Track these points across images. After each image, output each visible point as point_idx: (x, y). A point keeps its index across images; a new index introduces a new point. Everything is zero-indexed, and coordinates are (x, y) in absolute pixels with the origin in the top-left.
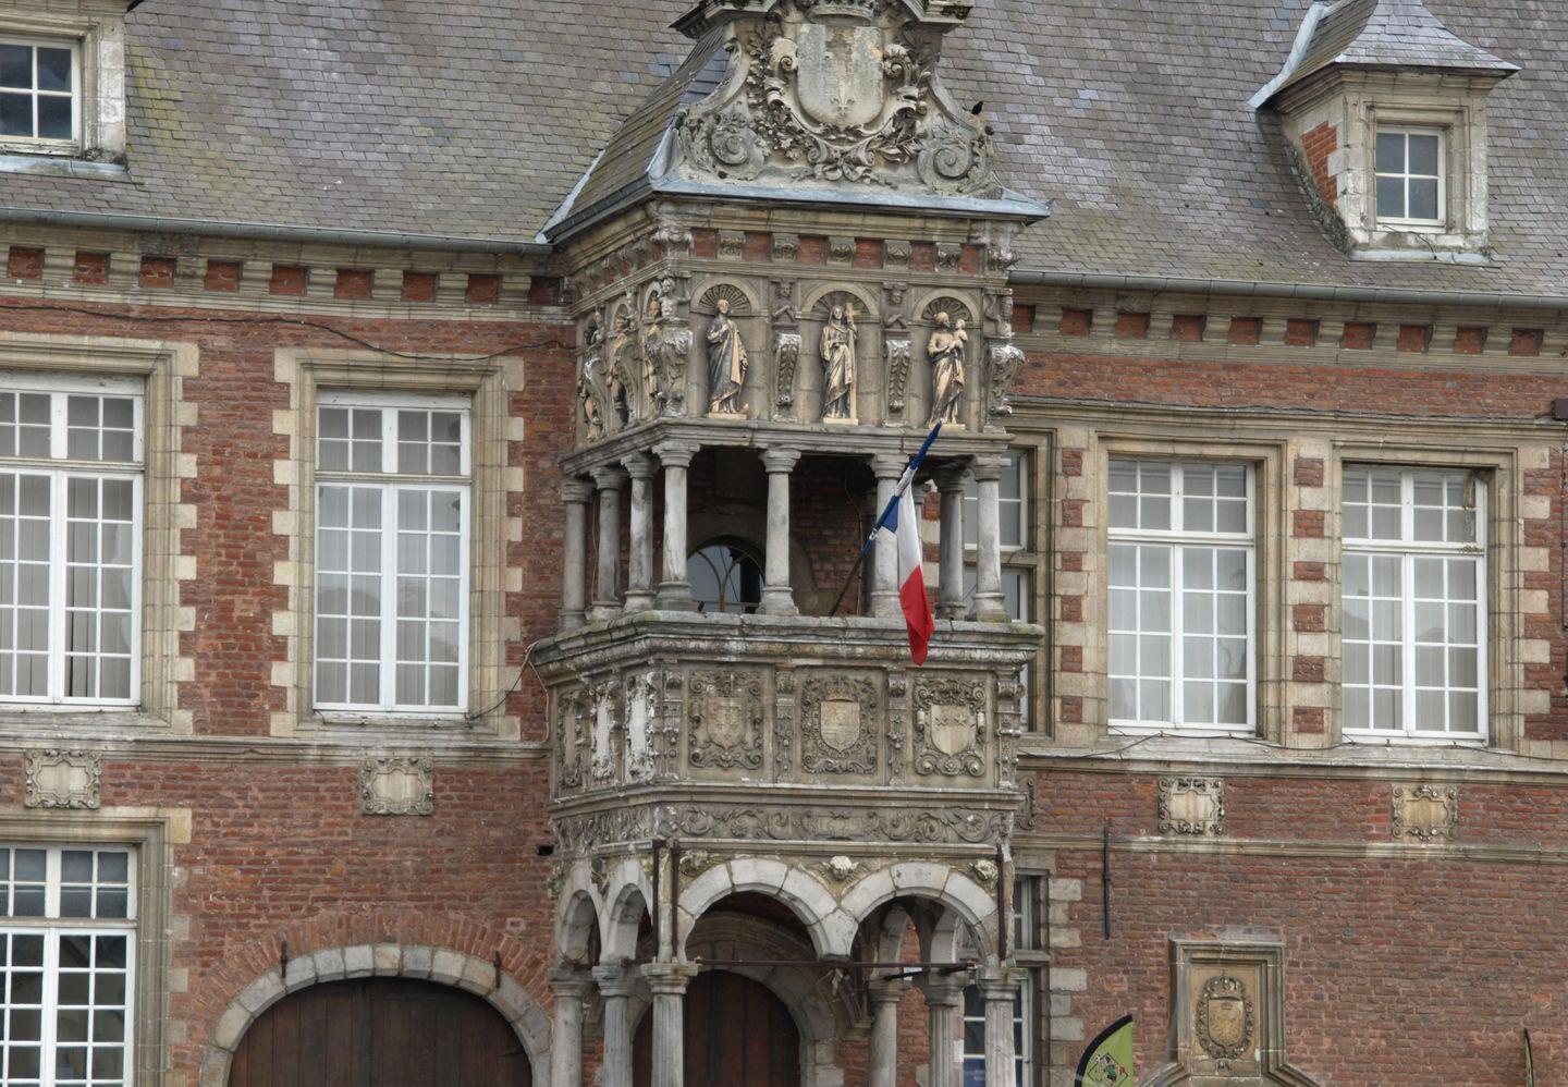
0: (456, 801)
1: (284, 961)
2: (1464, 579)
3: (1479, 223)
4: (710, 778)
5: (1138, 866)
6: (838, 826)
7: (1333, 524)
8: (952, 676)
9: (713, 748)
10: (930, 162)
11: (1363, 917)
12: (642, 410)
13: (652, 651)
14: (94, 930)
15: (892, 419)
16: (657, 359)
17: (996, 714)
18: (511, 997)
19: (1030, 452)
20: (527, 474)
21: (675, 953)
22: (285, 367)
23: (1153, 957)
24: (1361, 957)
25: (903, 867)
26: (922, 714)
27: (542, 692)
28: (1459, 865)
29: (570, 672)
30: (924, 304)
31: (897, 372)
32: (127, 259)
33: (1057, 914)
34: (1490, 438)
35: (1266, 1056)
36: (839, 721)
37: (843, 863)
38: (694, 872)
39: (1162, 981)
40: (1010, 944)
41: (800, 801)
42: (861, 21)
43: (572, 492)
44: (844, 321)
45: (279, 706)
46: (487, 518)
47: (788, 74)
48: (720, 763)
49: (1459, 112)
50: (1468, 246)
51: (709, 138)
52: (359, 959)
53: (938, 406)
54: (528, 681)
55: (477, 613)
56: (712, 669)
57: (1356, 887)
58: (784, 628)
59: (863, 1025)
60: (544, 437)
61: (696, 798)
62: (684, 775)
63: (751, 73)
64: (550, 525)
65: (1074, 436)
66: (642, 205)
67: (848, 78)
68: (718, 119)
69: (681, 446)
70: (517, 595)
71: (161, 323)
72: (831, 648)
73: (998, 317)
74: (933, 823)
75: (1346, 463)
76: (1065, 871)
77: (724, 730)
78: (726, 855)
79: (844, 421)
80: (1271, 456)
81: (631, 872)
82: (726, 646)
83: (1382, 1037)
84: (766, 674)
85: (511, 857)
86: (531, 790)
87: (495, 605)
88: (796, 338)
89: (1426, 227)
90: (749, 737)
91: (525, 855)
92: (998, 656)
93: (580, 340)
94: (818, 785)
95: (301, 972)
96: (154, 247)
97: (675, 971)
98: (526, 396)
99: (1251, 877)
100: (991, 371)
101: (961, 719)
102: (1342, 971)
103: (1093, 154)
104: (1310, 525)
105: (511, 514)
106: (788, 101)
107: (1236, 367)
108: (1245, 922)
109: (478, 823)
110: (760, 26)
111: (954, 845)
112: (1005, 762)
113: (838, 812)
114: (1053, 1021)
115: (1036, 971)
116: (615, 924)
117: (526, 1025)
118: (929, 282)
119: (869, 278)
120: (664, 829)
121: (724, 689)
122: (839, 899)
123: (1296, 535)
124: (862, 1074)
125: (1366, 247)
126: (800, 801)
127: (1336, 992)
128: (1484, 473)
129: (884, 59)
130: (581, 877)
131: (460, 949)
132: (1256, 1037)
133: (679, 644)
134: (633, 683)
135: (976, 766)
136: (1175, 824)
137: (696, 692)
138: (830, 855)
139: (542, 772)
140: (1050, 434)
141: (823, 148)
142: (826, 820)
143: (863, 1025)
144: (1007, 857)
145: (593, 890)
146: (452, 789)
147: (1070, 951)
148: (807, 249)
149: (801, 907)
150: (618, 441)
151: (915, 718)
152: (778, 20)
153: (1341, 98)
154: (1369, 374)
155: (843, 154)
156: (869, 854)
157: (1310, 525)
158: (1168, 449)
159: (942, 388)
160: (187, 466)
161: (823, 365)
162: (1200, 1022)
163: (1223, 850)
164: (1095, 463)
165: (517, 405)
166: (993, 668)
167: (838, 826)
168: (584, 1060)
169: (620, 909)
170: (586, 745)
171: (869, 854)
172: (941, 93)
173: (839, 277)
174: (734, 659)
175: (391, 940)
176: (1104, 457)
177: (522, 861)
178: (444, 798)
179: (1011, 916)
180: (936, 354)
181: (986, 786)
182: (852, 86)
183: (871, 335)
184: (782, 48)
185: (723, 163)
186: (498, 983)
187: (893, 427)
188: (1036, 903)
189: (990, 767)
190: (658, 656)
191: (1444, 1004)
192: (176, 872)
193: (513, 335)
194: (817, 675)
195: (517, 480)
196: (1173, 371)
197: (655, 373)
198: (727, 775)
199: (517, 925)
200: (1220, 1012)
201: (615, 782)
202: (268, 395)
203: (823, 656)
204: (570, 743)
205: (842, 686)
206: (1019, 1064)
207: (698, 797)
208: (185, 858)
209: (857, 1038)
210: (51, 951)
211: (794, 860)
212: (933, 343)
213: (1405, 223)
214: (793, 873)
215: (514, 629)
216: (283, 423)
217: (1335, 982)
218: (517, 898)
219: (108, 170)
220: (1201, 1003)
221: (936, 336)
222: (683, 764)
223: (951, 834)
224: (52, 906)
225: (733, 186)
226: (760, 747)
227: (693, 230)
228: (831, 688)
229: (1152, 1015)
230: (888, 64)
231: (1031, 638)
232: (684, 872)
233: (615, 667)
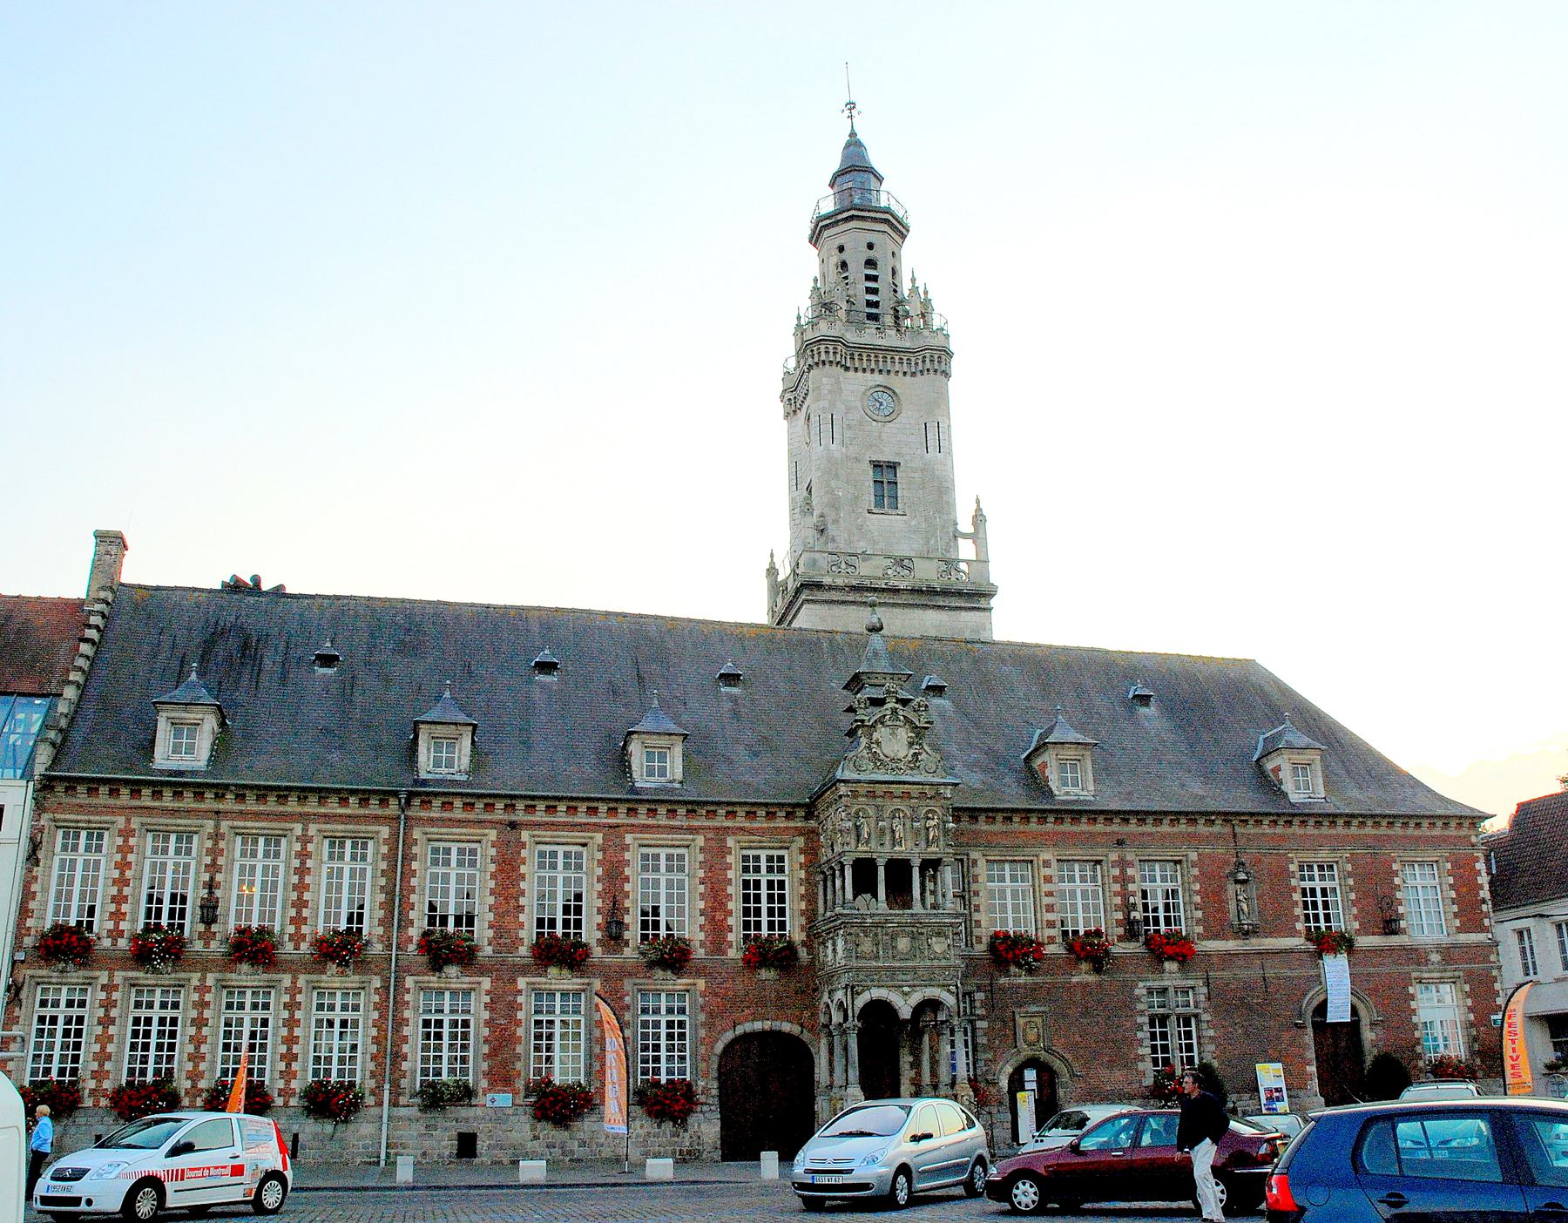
1: (734, 1027)
2: (1095, 895)
3: (1091, 788)
4: (862, 963)
5: (1002, 989)
6: (904, 977)
7: (1055, 879)
12: (838, 849)
13: (843, 923)
14: (676, 1018)
16: (841, 831)
18: (806, 1037)
19: (962, 860)
21: (854, 1020)
22: (730, 842)
23: (1008, 1014)
25: (926, 990)
30: (924, 812)
31: (917, 832)
32: (682, 811)
33: (978, 1004)
36: (903, 944)
37: (906, 989)
38: (858, 994)
40: (962, 1014)
42: (901, 727)
43: (819, 877)
44: (899, 817)
45: (731, 947)
47: (878, 743)
49: (1083, 755)
52: (758, 1026)
53: (930, 843)
54: (808, 936)
55: (792, 916)
62: (854, 963)
65: (974, 855)
66: (835, 784)
71: (692, 830)
75: (1058, 860)
76: (979, 989)
80: (1035, 858)
81: (839, 995)
87: (797, 913)
88: (884, 823)
89: (1077, 790)
92: (953, 921)
93: (820, 830)
95: (740, 1030)
96: (690, 807)
100: (946, 832)
103: (976, 772)
104: (1048, 879)
106: (878, 751)
115: (972, 1022)
125: (1059, 796)
128: (1099, 862)
130: (826, 996)
134: (838, 935)
138: (903, 986)
140: (968, 855)
144: (959, 985)
147: (983, 1016)
152: (874, 727)
154: (1064, 833)
157: (1048, 879)
158: (1003, 858)
159: (931, 838)
160: (701, 874)
161: (893, 831)
164: (982, 863)
165: (802, 851)
166: (951, 925)
167: (904, 977)
170: (825, 956)
172: (926, 747)
173: (897, 804)
175: (768, 1019)
176: (984, 861)
179: (962, 1005)
184: (876, 736)
186: (802, 1032)
187: (917, 850)
188: (971, 1000)
192: (700, 999)
194: (896, 929)
195: (803, 874)
199: (806, 1014)
202: (724, 851)
203: (898, 923)
204: (821, 955)
206: (967, 1053)
207: (859, 969)
208: (703, 995)
210: (663, 1025)
213: (1069, 789)
215: (803, 921)
216: (730, 859)
219: (677, 786)
222: (854, 960)
223: (941, 978)
224: (663, 1011)
225: (862, 777)
231: (962, 915)
232: (855, 994)
233: (833, 930)
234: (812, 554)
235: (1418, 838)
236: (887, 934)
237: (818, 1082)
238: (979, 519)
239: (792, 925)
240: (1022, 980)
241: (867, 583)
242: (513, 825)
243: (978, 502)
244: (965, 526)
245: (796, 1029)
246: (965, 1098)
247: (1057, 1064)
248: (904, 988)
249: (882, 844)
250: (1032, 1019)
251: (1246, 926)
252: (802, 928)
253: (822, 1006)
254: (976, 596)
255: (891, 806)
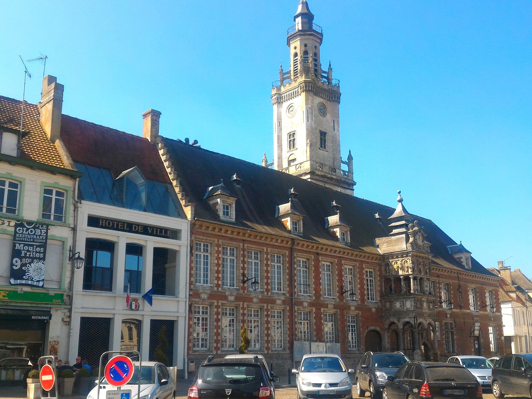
235: (347, 258)
238: (350, 158)
242: (317, 254)
243: (350, 152)
244: (345, 158)
254: (351, 185)
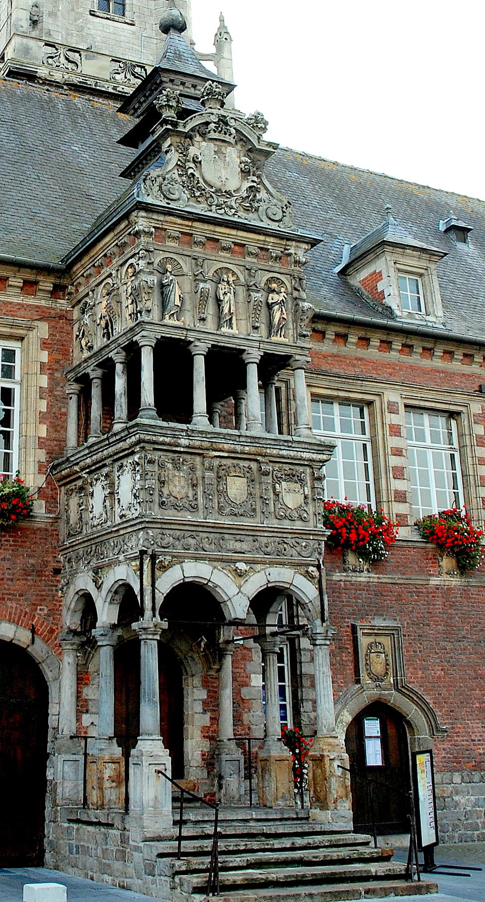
0: (12, 543)
3: (440, 313)
4: (170, 514)
6: (238, 546)
8: (291, 467)
9: (172, 498)
10: (264, 214)
11: (431, 613)
13: (139, 442)
15: (254, 333)
17: (313, 488)
18: (39, 650)
20: (49, 378)
21: (154, 616)
24: (431, 632)
26: (277, 485)
27: (56, 489)
28: (466, 588)
29: (77, 472)
30: (265, 279)
34: (459, 398)
35: (396, 681)
36: (236, 487)
37: (242, 566)
38: (164, 568)
39: (349, 644)
41: (219, 531)
44: (228, 282)
46: (29, 400)
47: (197, 162)
48: (175, 507)
50: (438, 322)
51: (160, 187)
53: (274, 330)
54: (49, 482)
55: (23, 447)
56: (171, 455)
57: (426, 598)
58: (209, 433)
59: (216, 667)
60: (57, 362)
61: (164, 526)
62: (156, 513)
63: (179, 160)
64: (60, 405)
67: (225, 168)
68: (164, 179)
69: (152, 335)
70: (44, 438)
72: (233, 446)
73: (300, 289)
74: (285, 546)
77: (178, 489)
78: (179, 559)
79: (230, 331)
80: (376, 398)
82: (179, 441)
83: (442, 670)
84: (198, 459)
85: (40, 574)
86: (50, 539)
87: (32, 443)
90: (190, 495)
91: (47, 573)
92: (315, 456)
94: (227, 521)
97: (155, 626)
98: (49, 341)
99: (384, 593)
101: (297, 490)
102: (424, 639)
104: (396, 431)
105: (41, 398)
106: (197, 174)
107: (360, 359)
108: (382, 615)
109: (23, 555)
110: (183, 139)
111: (296, 559)
112: (319, 514)
113: (238, 537)
114: (303, 664)
116: (107, 604)
117: (47, 665)
118: (267, 268)
119: (239, 263)
120: (146, 544)
121: (177, 466)
122: (240, 587)
123: (390, 435)
124: (216, 692)
126: (219, 531)
127: (422, 649)
129: (241, 163)
131: (14, 622)
132: (390, 671)
133: (154, 438)
135: (305, 515)
136: (351, 567)
137: (161, 466)
139: (56, 530)
141: (215, 198)
142: (232, 542)
143: (216, 667)
145: (92, 589)
146: (10, 536)
148: (210, 244)
149: (219, 591)
150: (108, 346)
151: (274, 488)
153: (384, 258)
155: (224, 202)
156: (254, 562)
159: (276, 320)
161: (218, 302)
162: (367, 664)
163: (371, 580)
165: (45, 345)
167: (238, 546)
168: (78, 684)
169: (110, 595)
171: (254, 562)
174: (182, 449)
177: (45, 576)
178: (5, 541)
180: (272, 303)
181: (310, 526)
182: (227, 172)
183: (241, 291)
184: (193, 151)
185: (168, 199)
187: (255, 336)
189: (311, 516)
190: (142, 445)
191: (465, 654)
193: (43, 312)
194: (224, 462)
195: (44, 381)
196: (335, 358)
197: (132, 303)
198: (179, 514)
200: (375, 660)
201: (109, 523)
205: (237, 468)
209: (213, 673)
211: (216, 564)
212: (270, 298)
214: (215, 571)
215: (42, 455)
217: (421, 644)
218: (43, 595)
220: (367, 655)
221: (271, 295)
226: (196, 499)
227: (154, 227)
228: (232, 469)
229: (346, 661)
230: (243, 165)
232: (158, 567)
234: (25, 40)
236: (210, 469)
237: (56, 729)
239: (23, 461)
240: (363, 578)
241: (91, 83)
243: (222, 20)
245: (22, 637)
246: (336, 763)
247: (412, 711)
248: (238, 565)
249: (203, 320)
250: (379, 639)
251: (342, 583)
252: (41, 468)
253: (70, 599)
255: (218, 261)
